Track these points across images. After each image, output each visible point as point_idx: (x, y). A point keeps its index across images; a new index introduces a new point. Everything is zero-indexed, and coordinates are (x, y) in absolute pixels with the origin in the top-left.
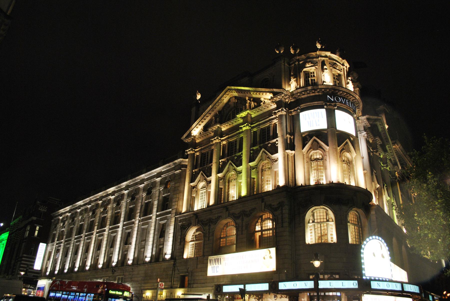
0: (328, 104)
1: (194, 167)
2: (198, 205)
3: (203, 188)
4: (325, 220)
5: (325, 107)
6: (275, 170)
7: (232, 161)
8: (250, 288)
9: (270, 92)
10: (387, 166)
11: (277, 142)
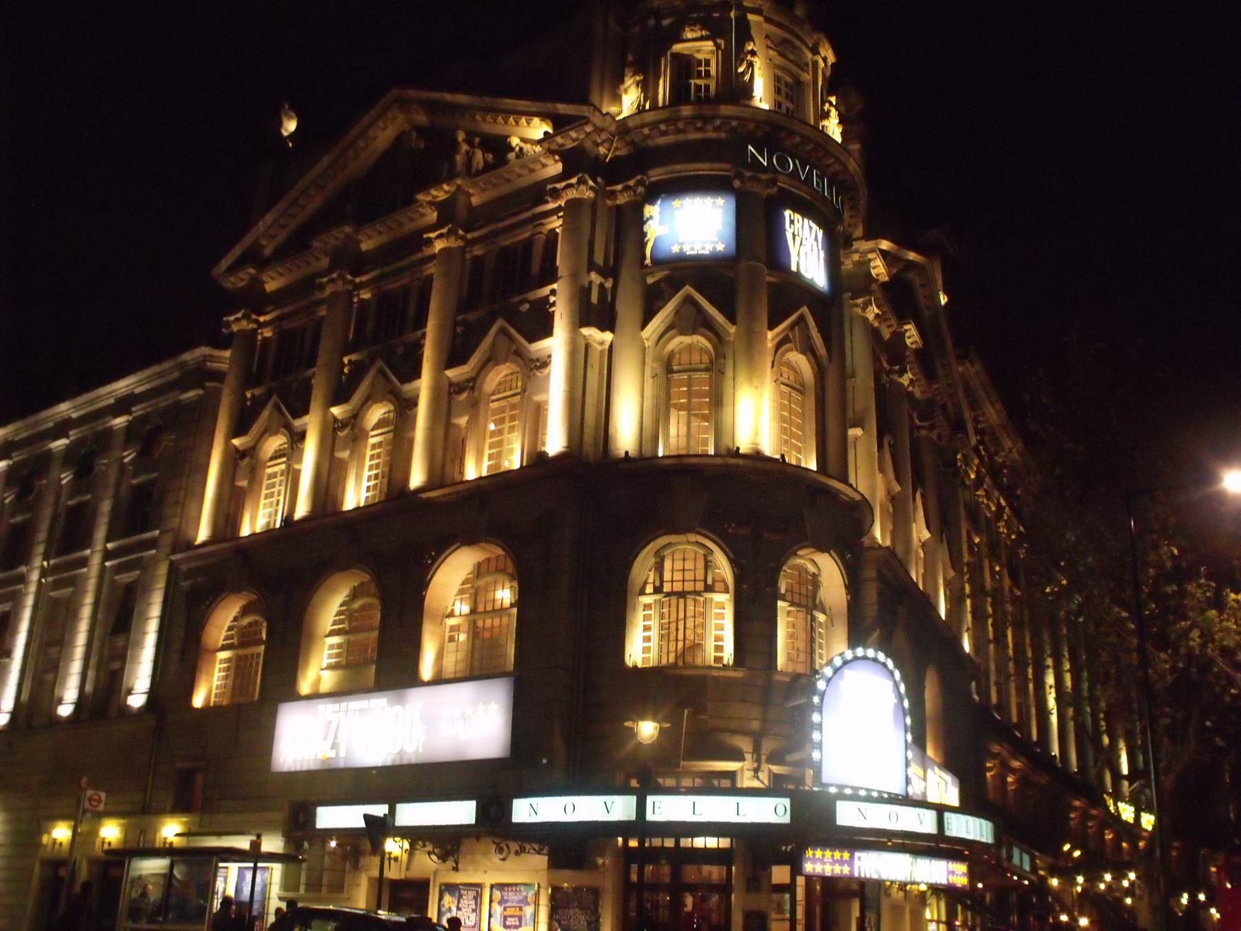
0: (748, 174)
1: (250, 380)
2: (253, 520)
3: (277, 455)
4: (700, 586)
5: (737, 184)
6: (538, 398)
7: (388, 362)
8: (412, 814)
9: (544, 116)
10: (931, 428)
11: (552, 299)
